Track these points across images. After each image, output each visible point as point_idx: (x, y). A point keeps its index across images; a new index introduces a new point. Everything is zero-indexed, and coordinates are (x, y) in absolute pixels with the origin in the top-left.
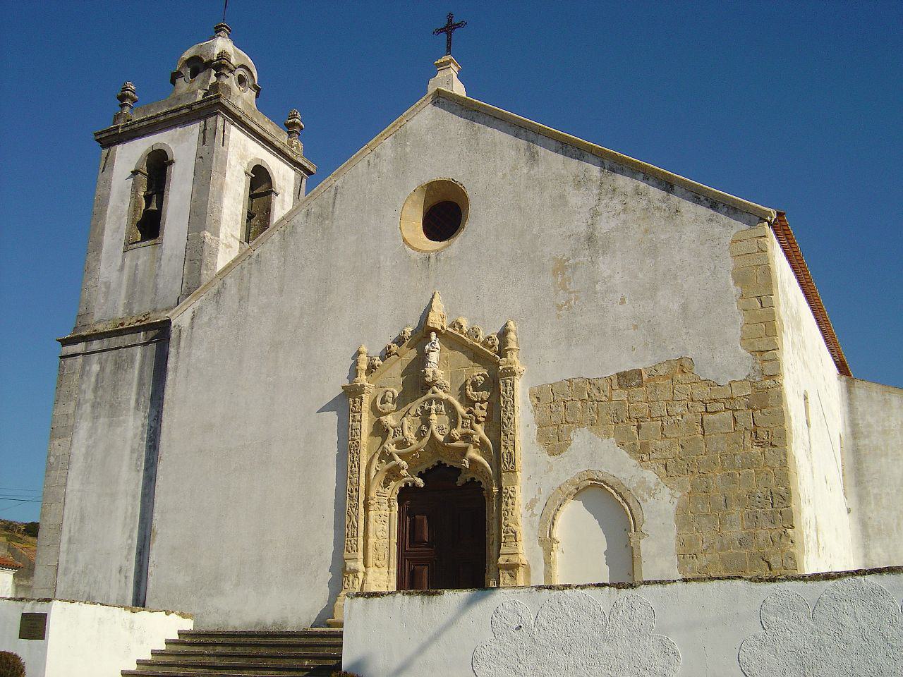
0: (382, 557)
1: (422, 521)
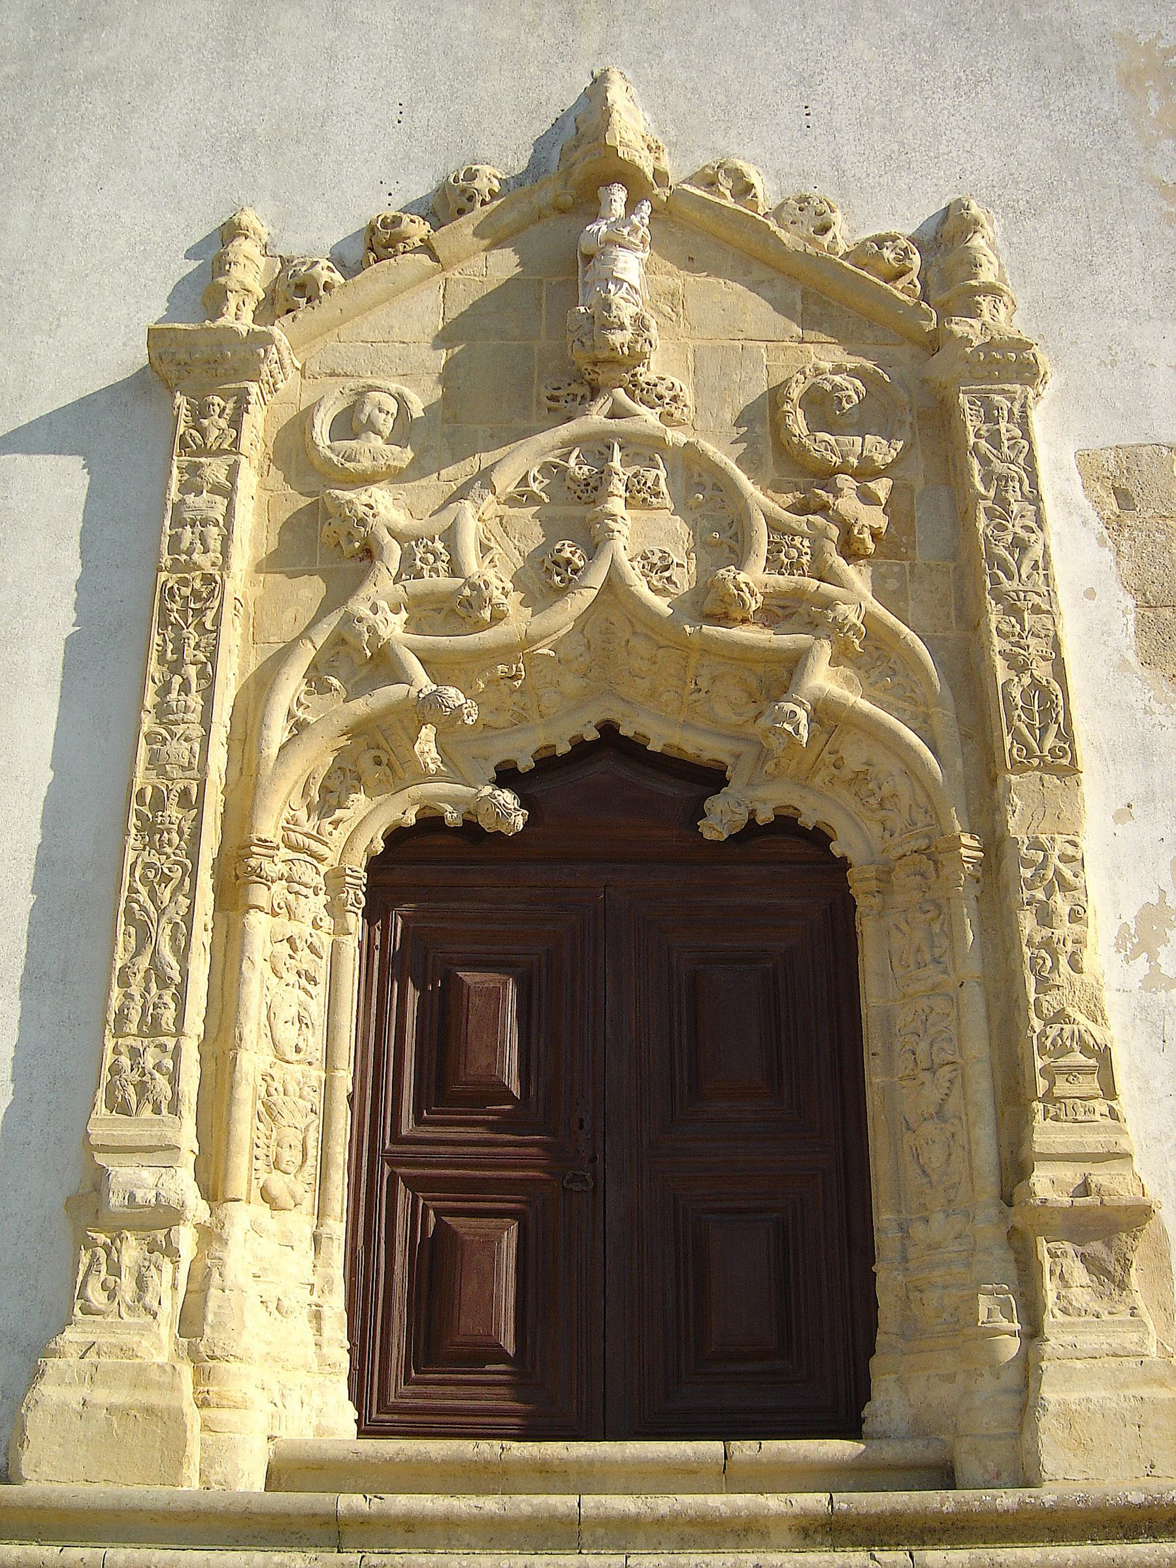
0: (291, 1156)
1: (495, 996)
